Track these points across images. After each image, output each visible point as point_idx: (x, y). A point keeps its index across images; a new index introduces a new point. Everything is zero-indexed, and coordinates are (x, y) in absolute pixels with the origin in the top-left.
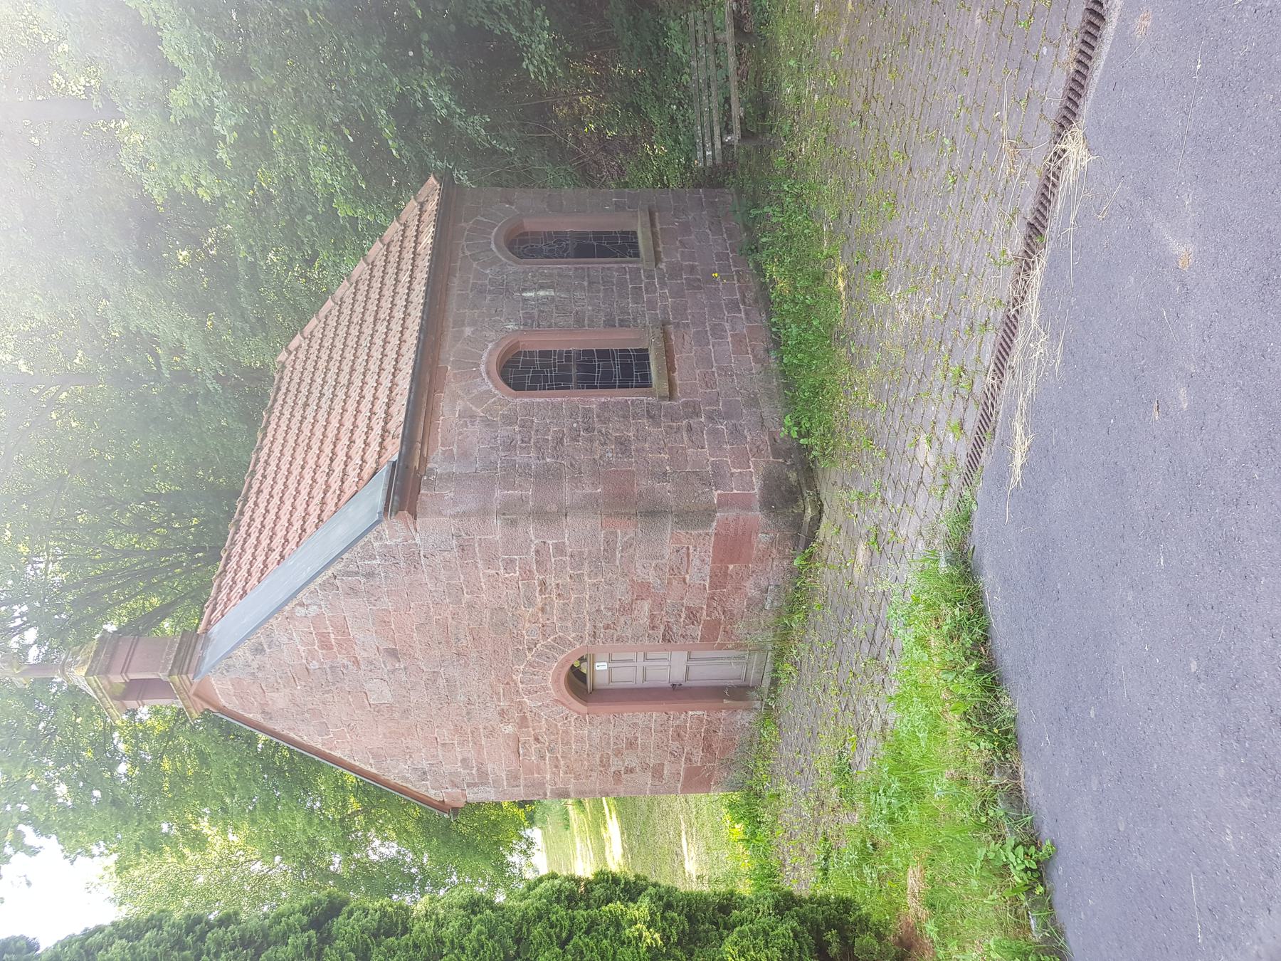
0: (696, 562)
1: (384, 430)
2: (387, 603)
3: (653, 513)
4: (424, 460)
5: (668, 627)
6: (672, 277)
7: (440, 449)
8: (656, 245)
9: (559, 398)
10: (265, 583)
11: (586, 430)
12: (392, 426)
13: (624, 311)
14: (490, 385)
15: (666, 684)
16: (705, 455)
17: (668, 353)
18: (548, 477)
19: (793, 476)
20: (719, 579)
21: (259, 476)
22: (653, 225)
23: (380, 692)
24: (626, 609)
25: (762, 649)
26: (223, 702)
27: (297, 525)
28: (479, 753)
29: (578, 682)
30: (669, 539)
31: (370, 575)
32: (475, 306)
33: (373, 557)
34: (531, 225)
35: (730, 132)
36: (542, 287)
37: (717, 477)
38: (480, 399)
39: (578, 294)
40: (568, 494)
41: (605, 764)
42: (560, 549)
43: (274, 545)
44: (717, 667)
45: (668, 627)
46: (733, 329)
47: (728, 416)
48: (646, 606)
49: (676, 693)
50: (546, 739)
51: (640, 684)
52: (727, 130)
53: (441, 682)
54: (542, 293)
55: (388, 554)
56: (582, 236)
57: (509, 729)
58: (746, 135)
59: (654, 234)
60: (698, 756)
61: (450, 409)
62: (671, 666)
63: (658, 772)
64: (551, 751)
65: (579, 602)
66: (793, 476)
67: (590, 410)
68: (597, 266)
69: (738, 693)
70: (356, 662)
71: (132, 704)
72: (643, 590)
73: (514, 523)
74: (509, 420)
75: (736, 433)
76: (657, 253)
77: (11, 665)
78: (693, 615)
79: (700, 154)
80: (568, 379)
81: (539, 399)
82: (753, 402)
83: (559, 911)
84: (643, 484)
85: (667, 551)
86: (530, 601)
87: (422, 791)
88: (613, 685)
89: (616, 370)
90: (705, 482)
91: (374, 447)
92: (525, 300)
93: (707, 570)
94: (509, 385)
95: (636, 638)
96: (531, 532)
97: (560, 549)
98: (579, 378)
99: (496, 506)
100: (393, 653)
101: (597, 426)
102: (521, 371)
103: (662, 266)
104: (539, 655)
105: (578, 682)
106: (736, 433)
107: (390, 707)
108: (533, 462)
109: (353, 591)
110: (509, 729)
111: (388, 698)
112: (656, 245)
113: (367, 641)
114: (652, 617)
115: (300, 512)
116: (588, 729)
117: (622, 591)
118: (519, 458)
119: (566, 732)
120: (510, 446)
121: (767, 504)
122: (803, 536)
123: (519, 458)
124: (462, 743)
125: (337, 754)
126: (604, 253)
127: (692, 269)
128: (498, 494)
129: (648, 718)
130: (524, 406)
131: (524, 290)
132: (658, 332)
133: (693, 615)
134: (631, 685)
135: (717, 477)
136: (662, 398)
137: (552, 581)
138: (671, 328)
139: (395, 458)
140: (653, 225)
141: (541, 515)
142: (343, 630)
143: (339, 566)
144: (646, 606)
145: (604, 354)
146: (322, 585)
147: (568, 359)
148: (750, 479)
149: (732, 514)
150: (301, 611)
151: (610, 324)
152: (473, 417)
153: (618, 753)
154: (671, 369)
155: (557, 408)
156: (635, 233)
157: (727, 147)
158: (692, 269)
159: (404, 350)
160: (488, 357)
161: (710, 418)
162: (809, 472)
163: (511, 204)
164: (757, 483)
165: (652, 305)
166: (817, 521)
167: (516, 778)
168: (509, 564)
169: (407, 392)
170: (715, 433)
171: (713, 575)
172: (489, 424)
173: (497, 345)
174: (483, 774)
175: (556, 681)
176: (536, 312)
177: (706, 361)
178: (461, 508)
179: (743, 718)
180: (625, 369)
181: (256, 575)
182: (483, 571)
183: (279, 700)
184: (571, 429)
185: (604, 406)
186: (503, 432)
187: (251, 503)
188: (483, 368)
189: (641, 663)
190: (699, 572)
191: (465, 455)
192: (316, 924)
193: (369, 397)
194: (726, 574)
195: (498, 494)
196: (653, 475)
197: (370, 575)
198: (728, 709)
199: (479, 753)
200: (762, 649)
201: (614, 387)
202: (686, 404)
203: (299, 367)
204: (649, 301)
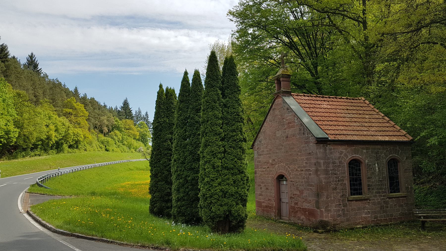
0: (308, 205)
1: (337, 134)
2: (298, 137)
3: (318, 195)
4: (329, 144)
5: (294, 198)
6: (384, 202)
7: (332, 147)
8: (394, 198)
9: (347, 174)
10: (302, 109)
11: (338, 180)
12: (338, 136)
13: (373, 189)
14: (350, 157)
15: (281, 197)
16: (333, 208)
17: (361, 200)
18: (326, 172)
19: (329, 228)
20: (304, 210)
21: (329, 99)
22: (401, 197)
23: (279, 134)
24: (297, 189)
25: (290, 220)
26: (276, 100)
27: (315, 114)
28: (265, 154)
29: (281, 178)
30: (312, 199)
31: (304, 134)
32: (372, 152)
33: (307, 134)
34: (400, 165)
35: (424, 218)
36: (379, 168)
37: (328, 211)
38: (346, 155)
39: (377, 178)
40: (322, 176)
41: (263, 183)
42: (310, 174)
43: (311, 109)
44: (285, 209)
45: (294, 198)
46: (369, 217)
47: (344, 214)
48: (298, 193)
49: (279, 200)
50: (268, 169)
51: (281, 191)
52: (424, 217)
53: (281, 147)
54: (377, 168)
55: (308, 138)
56: (397, 178)
57: (270, 161)
58: (424, 223)
59: (398, 197)
60: (264, 204)
61: (342, 149)
62: (285, 198)
63: (261, 195)
64: (265, 171)
65: (299, 178)
66: (329, 228)
67: (344, 181)
68: (387, 183)
69: (279, 213)
70: (285, 129)
71: (276, 82)
72: (301, 192)
73: (315, 165)
74: (340, 162)
75: (339, 215)
76: (392, 198)
77: (285, 234)
78: (296, 204)
79: (417, 210)
80: (353, 175)
81: (346, 169)
82: (348, 220)
83: (246, 178)
84: (325, 194)
85: (310, 198)
86: (299, 167)
87: (257, 141)
88: (281, 185)
89: (356, 187)
90: (327, 207)
91: (333, 132)
92: (375, 164)
93: (306, 207)
94: (350, 161)
95: (291, 191)
96: (313, 168)
97: (310, 174)
98: (353, 178)
99: (319, 161)
100: (287, 137)
101: (340, 183)
102: (354, 165)
103: (388, 199)
104: (287, 169)
105: (281, 178)
106: (339, 215)
107: (275, 136)
108: (330, 168)
109: (300, 130)
110: (270, 161)
111: (277, 135)
112: (394, 198)
113: (290, 132)
114: (296, 194)
115: (318, 114)
116: (271, 179)
117: (301, 188)
118: (331, 165)
119: (270, 174)
120: (334, 163)
121: (321, 221)
122: (315, 229)
123: (331, 165)
124: (267, 151)
125: (265, 123)
126: (391, 185)
127: (388, 207)
128: (322, 161)
129: (272, 192)
130: (344, 166)
131: (378, 164)
132: (366, 198)
133: (296, 204)
134: (281, 189)
135: (328, 211)
136: (348, 198)
137: (303, 172)
138: (369, 201)
139: (329, 139)
140: (401, 197)
141: (317, 171)
142: (293, 127)
143: (305, 127)
144: (298, 193)
145: (360, 184)
146: (301, 124)
147: (359, 175)
148: (327, 217)
149: (319, 213)
150: (296, 119)
151: (369, 185)
152: (341, 154)
153: (265, 186)
154: (356, 201)
155: (344, 173)
156: (399, 192)
157: (420, 217)
158: (388, 207)
159: (358, 136)
160: (358, 156)
161: (343, 210)
162: (328, 231)
163: (406, 159)
164: (326, 219)
165: (375, 196)
166: (318, 232)
167: (259, 162)
168: (306, 163)
169: (346, 139)
170: (339, 210)
171: (305, 209)
172: (339, 158)
173: (361, 158)
174: (260, 155)
175: (281, 172)
176: (371, 167)
177: (359, 209)
178: (318, 153)
179: (273, 215)
180: (356, 186)
181: (303, 105)
182: (304, 158)
183: (277, 112)
184: (339, 177)
185: (345, 184)
186: (337, 161)
187: (322, 99)
188: (354, 155)
189: (286, 192)
190: (306, 205)
191: (331, 153)
192: (244, 139)
193: (346, 128)
194: (305, 211)
195: (322, 161)
196: (328, 195)
197: (304, 134)
198: (275, 211)
199: (265, 154)
200: (290, 220)
201: (351, 186)
202: (346, 204)
203: (359, 104)
204: (376, 196)
